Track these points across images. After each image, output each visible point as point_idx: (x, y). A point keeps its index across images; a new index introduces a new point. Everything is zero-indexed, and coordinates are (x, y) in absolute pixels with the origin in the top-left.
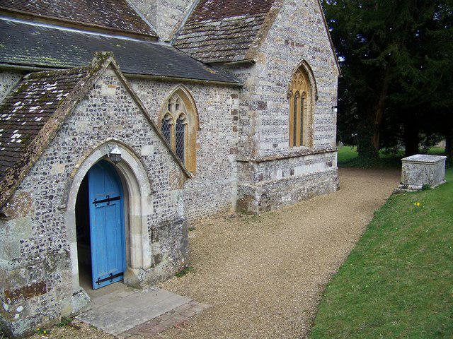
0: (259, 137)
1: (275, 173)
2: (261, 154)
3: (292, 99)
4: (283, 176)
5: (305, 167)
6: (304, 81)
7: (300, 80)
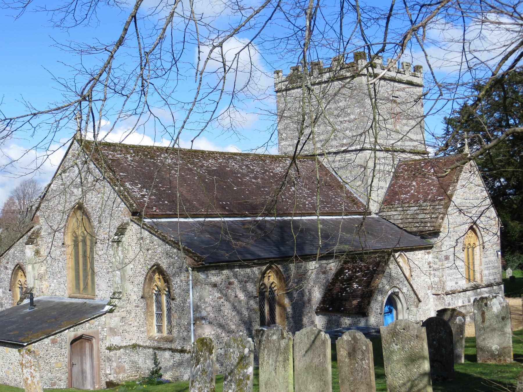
0: (446, 278)
1: (458, 302)
2: (448, 289)
3: (466, 250)
4: (463, 303)
5: (506, 62)
6: (474, 234)
7: (470, 235)
